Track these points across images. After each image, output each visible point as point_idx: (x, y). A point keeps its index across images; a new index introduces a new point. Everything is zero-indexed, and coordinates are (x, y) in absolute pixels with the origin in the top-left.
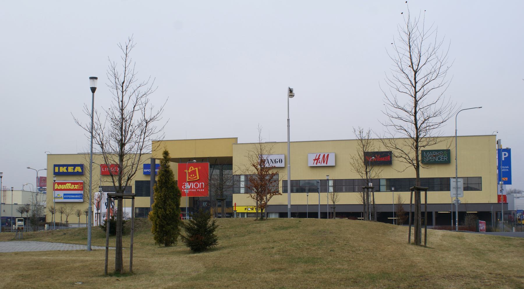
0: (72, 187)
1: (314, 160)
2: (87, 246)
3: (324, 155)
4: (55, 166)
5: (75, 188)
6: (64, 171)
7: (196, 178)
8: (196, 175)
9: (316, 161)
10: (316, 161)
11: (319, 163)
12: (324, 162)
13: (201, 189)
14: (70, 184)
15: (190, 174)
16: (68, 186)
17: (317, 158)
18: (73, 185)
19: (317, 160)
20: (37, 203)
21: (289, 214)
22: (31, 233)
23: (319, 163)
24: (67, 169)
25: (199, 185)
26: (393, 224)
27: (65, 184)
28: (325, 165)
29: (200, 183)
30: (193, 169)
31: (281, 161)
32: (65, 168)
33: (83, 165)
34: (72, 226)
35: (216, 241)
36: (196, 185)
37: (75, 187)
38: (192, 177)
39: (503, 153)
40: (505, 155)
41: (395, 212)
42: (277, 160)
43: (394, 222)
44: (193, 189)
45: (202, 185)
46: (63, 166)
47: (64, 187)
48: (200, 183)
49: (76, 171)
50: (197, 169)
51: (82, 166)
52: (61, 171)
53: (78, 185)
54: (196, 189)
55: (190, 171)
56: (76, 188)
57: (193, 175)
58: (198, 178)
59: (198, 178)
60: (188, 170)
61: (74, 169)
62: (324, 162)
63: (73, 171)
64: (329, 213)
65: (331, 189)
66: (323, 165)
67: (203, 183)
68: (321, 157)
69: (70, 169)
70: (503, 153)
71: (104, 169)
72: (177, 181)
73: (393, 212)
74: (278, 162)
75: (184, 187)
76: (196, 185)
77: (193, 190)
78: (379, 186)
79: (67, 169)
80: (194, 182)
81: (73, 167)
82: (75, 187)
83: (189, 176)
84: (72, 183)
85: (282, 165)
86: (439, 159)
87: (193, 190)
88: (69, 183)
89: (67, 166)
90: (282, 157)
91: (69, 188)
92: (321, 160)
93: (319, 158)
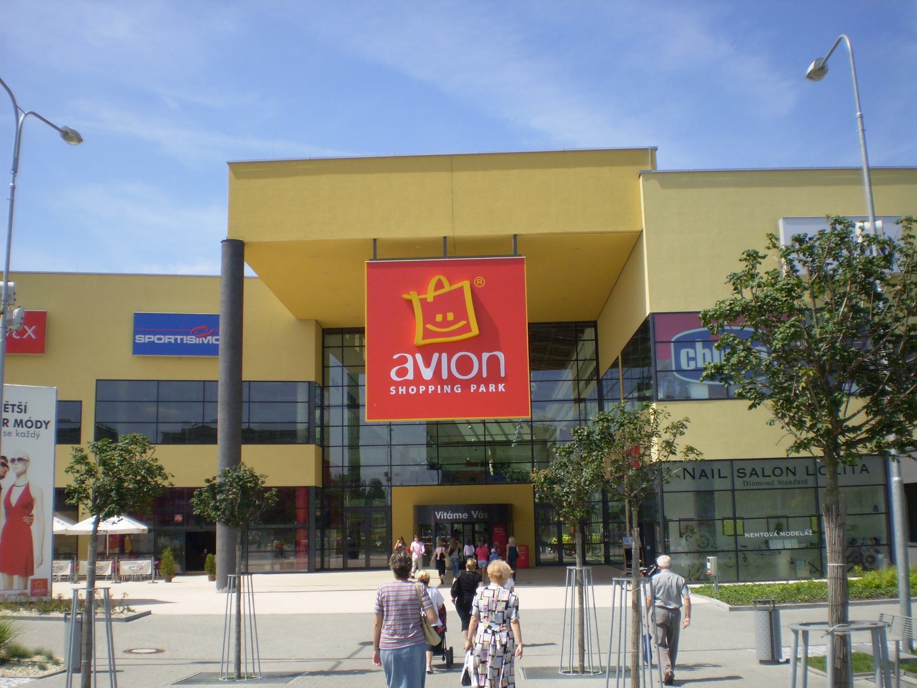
7: (467, 328)
8: (461, 314)
13: (487, 383)
15: (429, 310)
25: (479, 364)
30: (447, 288)
36: (464, 365)
38: (445, 323)
48: (485, 356)
50: (466, 285)
54: (465, 385)
55: (430, 296)
57: (450, 316)
59: (475, 331)
60: (422, 289)
67: (501, 355)
76: (464, 365)
77: (447, 389)
80: (450, 348)
83: (428, 318)
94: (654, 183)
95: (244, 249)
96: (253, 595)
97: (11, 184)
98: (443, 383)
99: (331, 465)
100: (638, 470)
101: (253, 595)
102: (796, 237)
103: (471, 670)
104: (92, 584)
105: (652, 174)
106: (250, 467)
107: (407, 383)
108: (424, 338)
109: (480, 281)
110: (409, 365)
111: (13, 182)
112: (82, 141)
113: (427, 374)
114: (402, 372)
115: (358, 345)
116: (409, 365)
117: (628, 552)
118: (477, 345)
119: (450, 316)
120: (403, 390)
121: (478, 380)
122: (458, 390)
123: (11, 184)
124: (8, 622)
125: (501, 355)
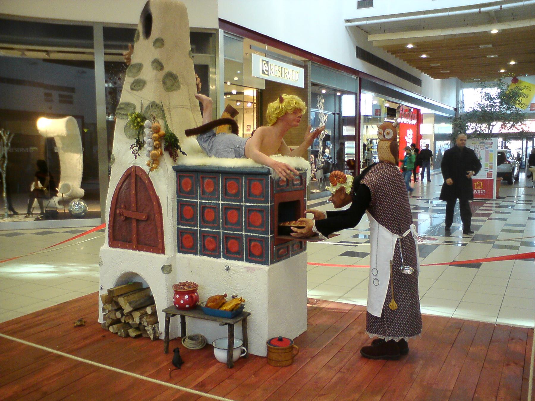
8: (481, 186)
15: (477, 185)
20: (371, 148)
21: (98, 36)
22: (306, 235)
25: (482, 191)
26: (198, 255)
30: (479, 183)
35: (519, 97)
36: (481, 191)
43: (198, 225)
50: (481, 183)
55: (477, 184)
58: (482, 188)
59: (482, 188)
60: (476, 183)
64: (71, 97)
76: (481, 191)
78: (377, 148)
80: (479, 190)
83: (477, 186)
99: (227, 351)
100: (432, 227)
102: (430, 231)
103: (151, 108)
106: (133, 154)
108: (419, 246)
112: (376, 110)
113: (476, 192)
117: (153, 306)
118: (482, 189)
124: (528, 155)
125: (485, 191)
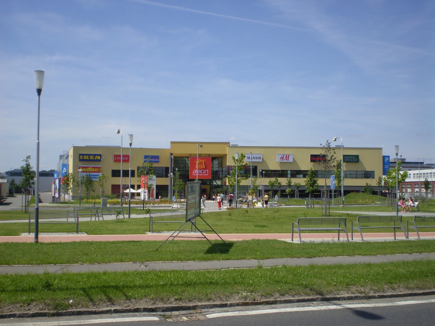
0: (93, 170)
1: (281, 158)
2: (337, 240)
3: (287, 156)
4: (80, 155)
5: (95, 171)
6: (87, 159)
7: (203, 167)
8: (203, 165)
9: (281, 159)
10: (281, 159)
11: (284, 160)
12: (286, 160)
13: (205, 174)
14: (91, 168)
16: (90, 169)
17: (282, 157)
18: (94, 169)
19: (282, 158)
23: (284, 160)
24: (89, 157)
25: (205, 171)
27: (88, 167)
28: (287, 161)
29: (205, 170)
30: (201, 161)
31: (259, 158)
32: (88, 156)
33: (101, 155)
34: (203, 212)
36: (203, 172)
37: (95, 170)
38: (200, 166)
39: (386, 158)
40: (387, 159)
41: (341, 196)
42: (257, 157)
44: (200, 174)
45: (207, 171)
46: (86, 155)
47: (87, 170)
48: (205, 170)
49: (96, 159)
50: (203, 161)
51: (100, 155)
52: (85, 158)
53: (97, 169)
54: (203, 174)
56: (96, 171)
57: (201, 165)
58: (204, 167)
59: (204, 167)
61: (94, 157)
62: (286, 160)
63: (93, 159)
65: (289, 176)
66: (286, 161)
67: (208, 171)
68: (285, 156)
69: (92, 158)
70: (386, 158)
71: (116, 158)
72: (168, 168)
73: (120, 185)
74: (258, 159)
75: (194, 172)
76: (203, 172)
77: (200, 175)
79: (89, 157)
80: (201, 169)
81: (93, 156)
82: (95, 170)
84: (93, 167)
85: (261, 160)
86: (353, 160)
87: (200, 175)
88: (90, 167)
89: (89, 155)
90: (261, 156)
91: (91, 171)
92: (284, 158)
93: (283, 157)
94: (229, 147)
95: (302, 170)
96: (150, 229)
97: (37, 141)
98: (200, 174)
101: (150, 229)
104: (143, 206)
105: (229, 146)
107: (195, 174)
109: (205, 160)
110: (195, 171)
111: (38, 140)
114: (194, 172)
115: (33, 235)
116: (195, 171)
118: (204, 169)
119: (201, 165)
120: (194, 175)
121: (204, 173)
122: (202, 175)
123: (37, 141)
125: (208, 171)
